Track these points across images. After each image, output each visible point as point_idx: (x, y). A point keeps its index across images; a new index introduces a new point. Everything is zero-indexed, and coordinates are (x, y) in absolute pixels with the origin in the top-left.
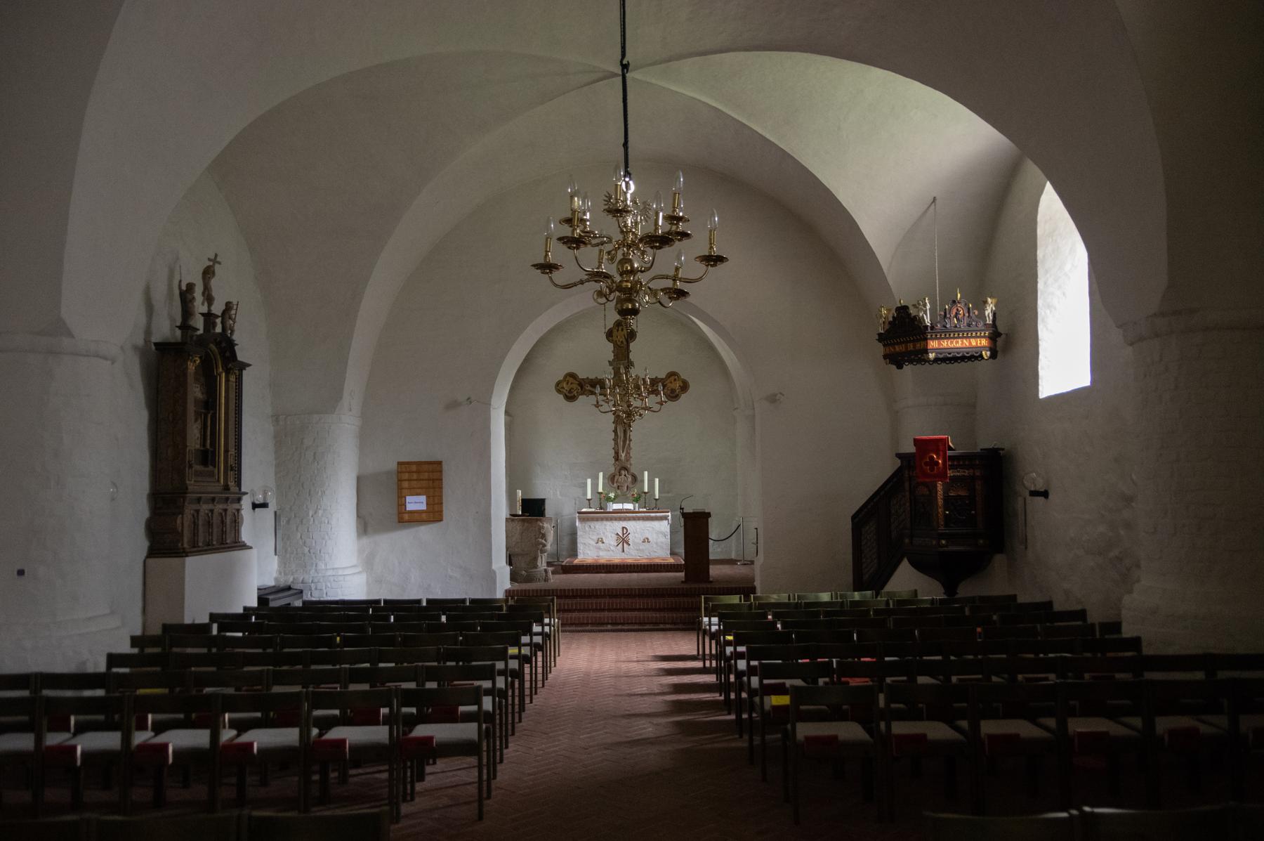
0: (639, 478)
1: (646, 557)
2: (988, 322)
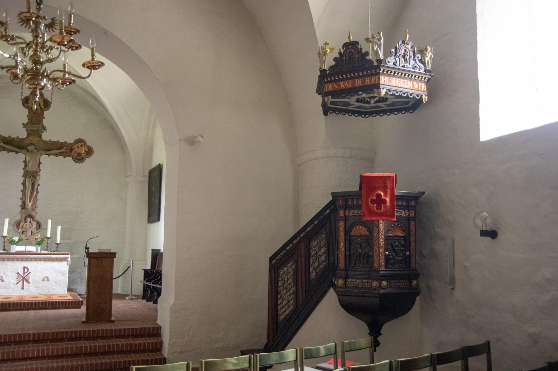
0: (43, 226)
1: (44, 293)
2: (427, 68)
